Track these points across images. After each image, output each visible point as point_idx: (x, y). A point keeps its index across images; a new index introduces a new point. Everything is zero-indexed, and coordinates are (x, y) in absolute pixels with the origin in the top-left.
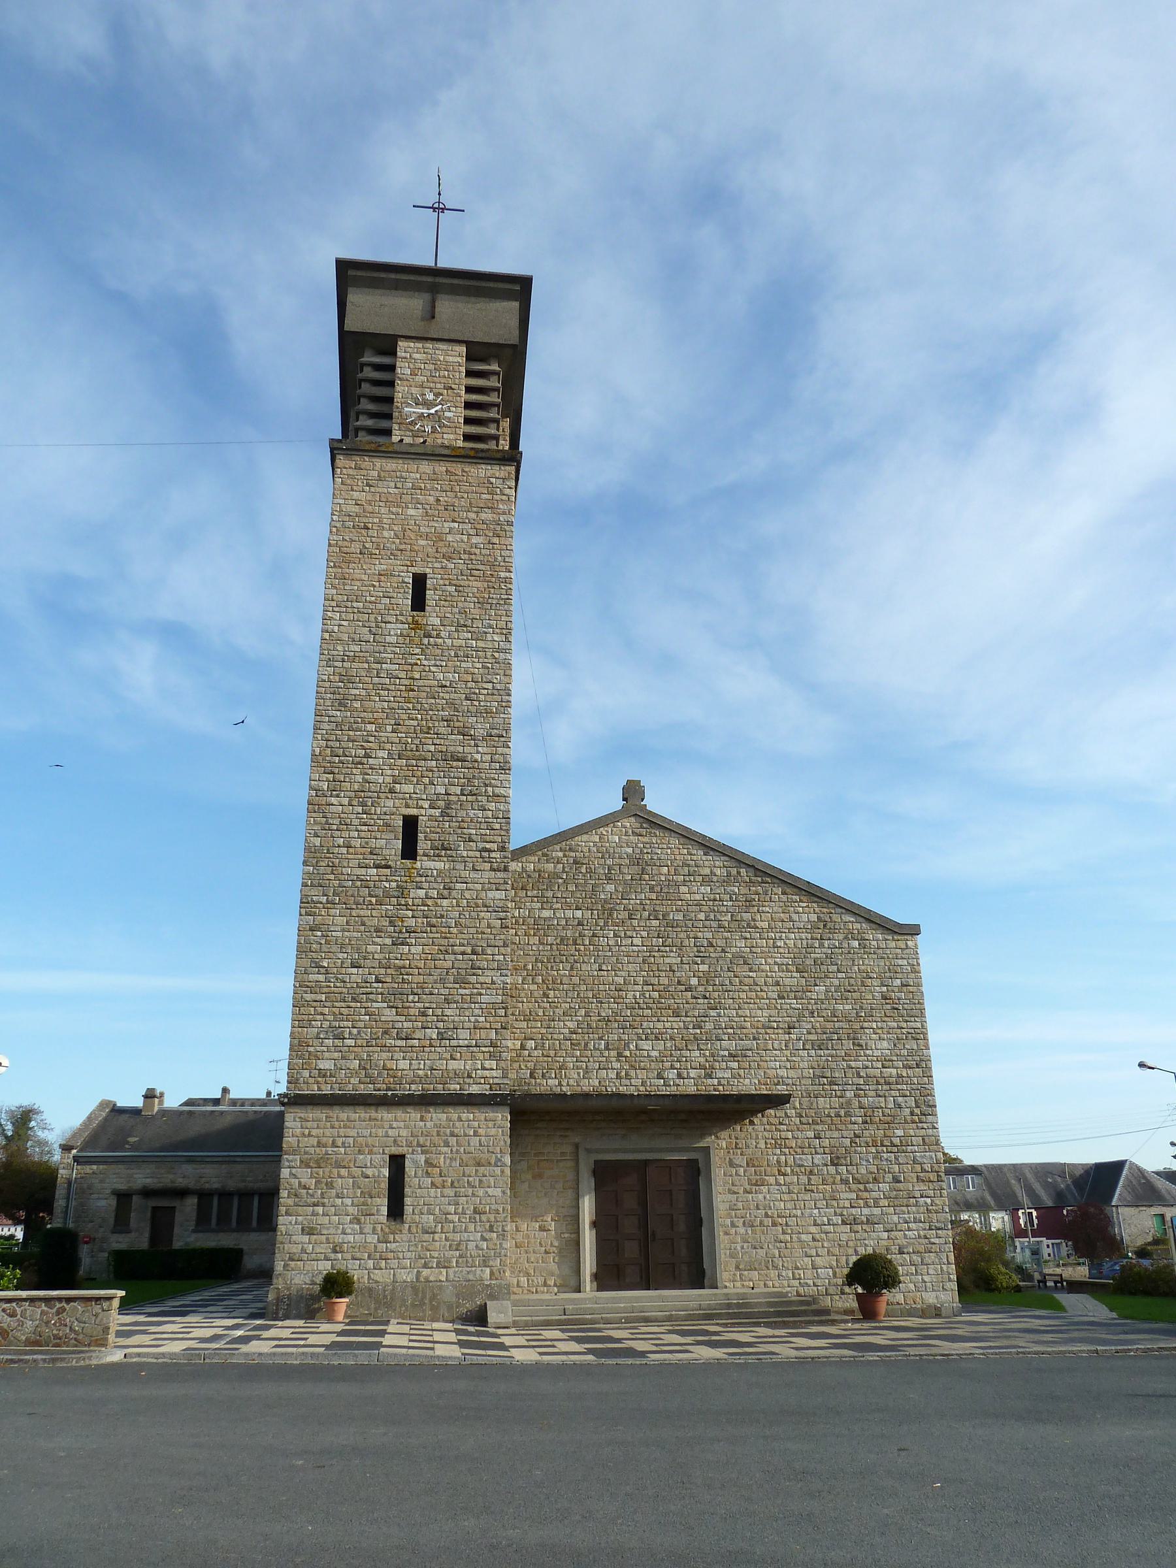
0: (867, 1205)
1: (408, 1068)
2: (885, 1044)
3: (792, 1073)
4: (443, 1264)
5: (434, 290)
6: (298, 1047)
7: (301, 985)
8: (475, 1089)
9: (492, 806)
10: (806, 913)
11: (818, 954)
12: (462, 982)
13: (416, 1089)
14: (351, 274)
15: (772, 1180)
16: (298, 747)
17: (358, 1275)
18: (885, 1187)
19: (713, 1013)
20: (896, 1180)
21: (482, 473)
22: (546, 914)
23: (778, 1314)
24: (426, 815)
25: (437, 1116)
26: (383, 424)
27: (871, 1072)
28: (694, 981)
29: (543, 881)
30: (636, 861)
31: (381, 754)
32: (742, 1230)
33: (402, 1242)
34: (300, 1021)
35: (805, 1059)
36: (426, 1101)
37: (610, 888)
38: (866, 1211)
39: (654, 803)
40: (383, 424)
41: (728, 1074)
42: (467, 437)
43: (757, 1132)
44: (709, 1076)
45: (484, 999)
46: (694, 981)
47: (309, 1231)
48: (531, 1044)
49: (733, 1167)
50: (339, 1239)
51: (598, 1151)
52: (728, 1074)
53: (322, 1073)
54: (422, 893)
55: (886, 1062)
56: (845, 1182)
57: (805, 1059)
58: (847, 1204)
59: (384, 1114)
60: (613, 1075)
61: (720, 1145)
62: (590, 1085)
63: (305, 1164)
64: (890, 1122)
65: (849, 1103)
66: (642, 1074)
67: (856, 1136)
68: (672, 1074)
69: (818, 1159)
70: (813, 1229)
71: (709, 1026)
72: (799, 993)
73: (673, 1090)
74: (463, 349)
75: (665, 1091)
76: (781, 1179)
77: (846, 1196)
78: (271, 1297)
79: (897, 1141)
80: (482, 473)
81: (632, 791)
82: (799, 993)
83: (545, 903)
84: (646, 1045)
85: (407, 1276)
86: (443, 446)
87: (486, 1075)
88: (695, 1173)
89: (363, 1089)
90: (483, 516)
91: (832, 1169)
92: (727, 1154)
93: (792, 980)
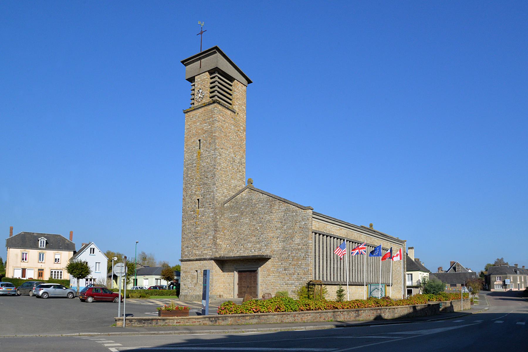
6: (182, 250)
8: (208, 257)
10: (284, 206)
12: (206, 234)
24: (200, 198)
28: (258, 228)
35: (281, 245)
37: (243, 207)
39: (255, 186)
46: (258, 228)
47: (185, 285)
55: (299, 244)
56: (287, 275)
62: (238, 254)
64: (298, 260)
65: (289, 255)
66: (248, 251)
68: (253, 251)
72: (280, 228)
73: (253, 254)
74: (207, 73)
77: (286, 278)
78: (260, 296)
81: (250, 182)
82: (280, 228)
87: (209, 254)
93: (279, 225)
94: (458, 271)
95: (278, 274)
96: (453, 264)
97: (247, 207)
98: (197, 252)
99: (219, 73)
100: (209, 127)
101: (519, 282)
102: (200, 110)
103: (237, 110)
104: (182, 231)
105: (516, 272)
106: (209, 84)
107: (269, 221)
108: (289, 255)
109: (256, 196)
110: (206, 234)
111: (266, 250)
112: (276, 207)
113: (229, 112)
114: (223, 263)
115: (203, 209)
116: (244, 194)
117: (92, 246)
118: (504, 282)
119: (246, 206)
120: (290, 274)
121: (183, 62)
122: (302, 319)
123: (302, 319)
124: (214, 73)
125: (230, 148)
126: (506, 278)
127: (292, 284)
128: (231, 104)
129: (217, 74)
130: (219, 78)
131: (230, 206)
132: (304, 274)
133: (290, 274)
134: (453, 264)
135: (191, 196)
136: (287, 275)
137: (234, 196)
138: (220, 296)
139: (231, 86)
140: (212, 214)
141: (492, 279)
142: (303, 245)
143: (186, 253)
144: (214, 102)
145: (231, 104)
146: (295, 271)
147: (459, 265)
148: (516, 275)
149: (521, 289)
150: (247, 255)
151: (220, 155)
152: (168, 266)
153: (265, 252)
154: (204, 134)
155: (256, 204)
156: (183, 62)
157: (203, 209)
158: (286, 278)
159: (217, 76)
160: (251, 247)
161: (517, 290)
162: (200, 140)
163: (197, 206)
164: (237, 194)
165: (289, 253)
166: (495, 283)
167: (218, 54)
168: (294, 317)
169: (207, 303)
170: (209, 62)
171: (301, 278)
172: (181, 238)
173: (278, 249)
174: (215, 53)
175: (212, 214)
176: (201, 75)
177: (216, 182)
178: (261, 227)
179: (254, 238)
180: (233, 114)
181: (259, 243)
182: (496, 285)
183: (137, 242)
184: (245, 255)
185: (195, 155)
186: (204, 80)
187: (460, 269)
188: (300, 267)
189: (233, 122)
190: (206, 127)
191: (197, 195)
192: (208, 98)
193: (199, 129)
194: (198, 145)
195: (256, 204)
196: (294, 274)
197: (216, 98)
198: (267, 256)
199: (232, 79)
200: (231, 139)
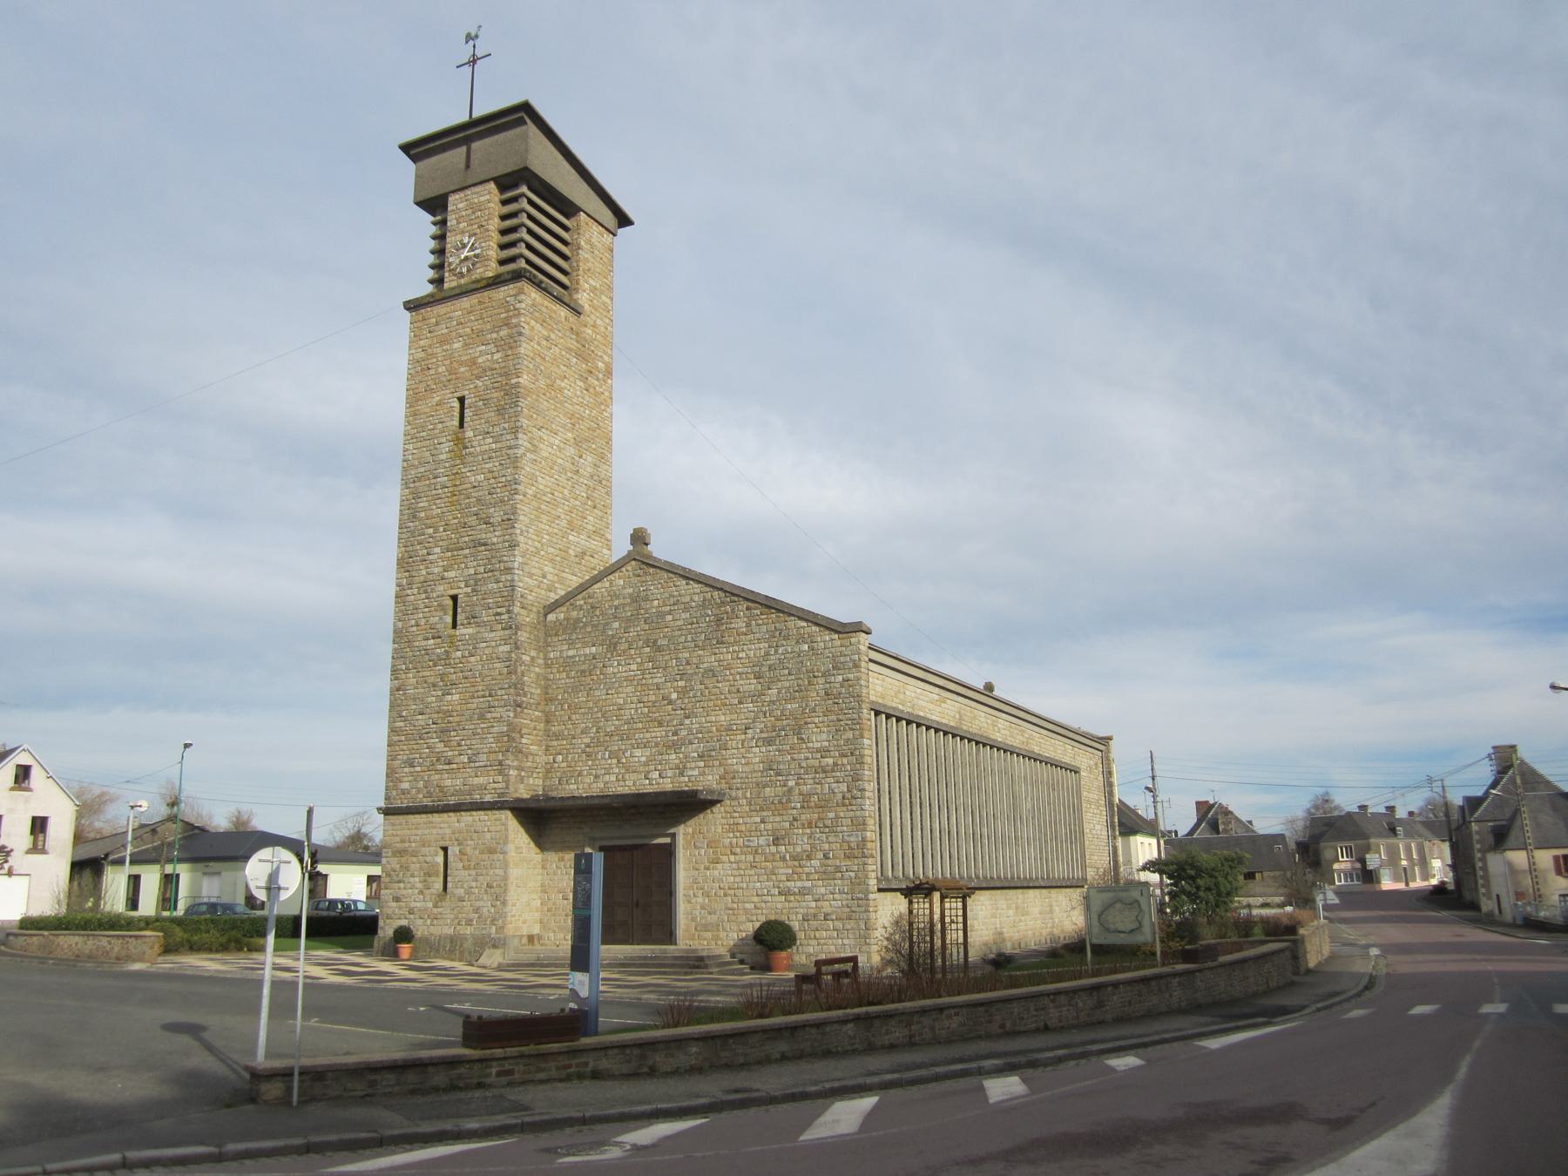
0: (800, 879)
1: (453, 784)
2: (824, 736)
3: (746, 768)
4: (469, 922)
5: (467, 141)
6: (391, 773)
7: (393, 730)
8: (488, 798)
9: (503, 578)
11: (773, 659)
12: (482, 717)
13: (452, 800)
14: (416, 150)
15: (725, 858)
16: (390, 552)
17: (420, 929)
18: (815, 863)
19: (687, 721)
20: (826, 857)
21: (501, 295)
22: (571, 653)
23: (682, 966)
24: (462, 591)
25: (467, 818)
26: (509, 223)
27: (811, 762)
28: (674, 696)
29: (571, 626)
30: (635, 599)
31: (437, 550)
32: (700, 900)
33: (446, 909)
34: (392, 757)
35: (757, 755)
36: (457, 808)
37: (616, 625)
38: (799, 884)
40: (509, 223)
41: (696, 772)
42: (502, 262)
43: (713, 821)
44: (682, 774)
45: (495, 730)
46: (674, 696)
47: (397, 899)
48: (560, 758)
49: (690, 845)
50: (413, 905)
51: (603, 839)
52: (696, 772)
53: (404, 792)
54: (459, 654)
55: (824, 752)
56: (783, 859)
57: (757, 755)
58: (784, 878)
59: (436, 818)
60: (613, 778)
61: (684, 833)
63: (394, 854)
64: (823, 805)
65: (790, 790)
66: (634, 776)
67: (795, 819)
69: (762, 841)
70: (755, 899)
71: (683, 733)
74: (492, 185)
75: (649, 789)
76: (732, 858)
77: (783, 871)
79: (829, 823)
80: (501, 295)
82: (757, 696)
83: (571, 644)
84: (638, 753)
85: (449, 931)
86: (477, 281)
88: (669, 851)
89: (427, 802)
90: (502, 333)
91: (773, 849)
92: (686, 837)
93: (751, 685)
94: (1225, 831)
95: (750, 858)
96: (1204, 808)
97: (629, 622)
98: (448, 782)
99: (530, 189)
100: (497, 356)
101: (1404, 863)
102: (466, 302)
103: (587, 307)
104: (392, 706)
105: (1393, 831)
106: (497, 220)
107: (711, 672)
108: (790, 790)
109: (658, 590)
110: (482, 717)
111: (703, 774)
112: (740, 624)
113: (563, 312)
114: (542, 819)
115: (470, 631)
116: (618, 580)
117: (24, 759)
118: (1363, 861)
119: (628, 620)
120: (794, 858)
121: (407, 148)
122: (932, 1029)
123: (932, 1029)
124: (516, 186)
125: (564, 426)
126: (1368, 849)
127: (803, 892)
128: (564, 287)
129: (524, 189)
130: (531, 202)
131: (567, 619)
132: (847, 857)
133: (794, 858)
134: (1204, 808)
135: (426, 587)
136: (783, 859)
137: (583, 588)
138: (531, 939)
139: (566, 228)
140: (507, 648)
141: (1327, 854)
142: (843, 755)
143: (405, 786)
144: (517, 276)
145: (564, 287)
146: (813, 846)
147: (1227, 812)
148: (1392, 841)
149: (1413, 885)
150: (633, 790)
151: (535, 450)
152: (247, 823)
153: (703, 779)
154: (478, 378)
155: (662, 615)
156: (407, 148)
157: (470, 631)
158: (783, 871)
159: (523, 195)
160: (646, 764)
161: (1401, 886)
162: (462, 400)
163: (449, 619)
164: (596, 580)
165: (791, 783)
166: (1336, 866)
167: (531, 128)
168: (909, 1024)
169: (593, 984)
170: (492, 152)
171: (838, 869)
172: (385, 730)
173: (746, 768)
174: (521, 122)
175: (507, 648)
176: (468, 192)
177: (521, 539)
178: (683, 692)
179: (659, 733)
180: (572, 318)
181: (674, 746)
182: (1339, 872)
183: (187, 746)
184: (626, 791)
185: (446, 447)
186: (476, 208)
187: (1232, 825)
188: (832, 829)
189: (574, 345)
190: (486, 355)
191: (452, 583)
192: (494, 264)
193: (461, 364)
194: (457, 414)
195: (662, 615)
196: (809, 858)
197: (522, 264)
198: (712, 792)
199: (569, 208)
200: (570, 398)
